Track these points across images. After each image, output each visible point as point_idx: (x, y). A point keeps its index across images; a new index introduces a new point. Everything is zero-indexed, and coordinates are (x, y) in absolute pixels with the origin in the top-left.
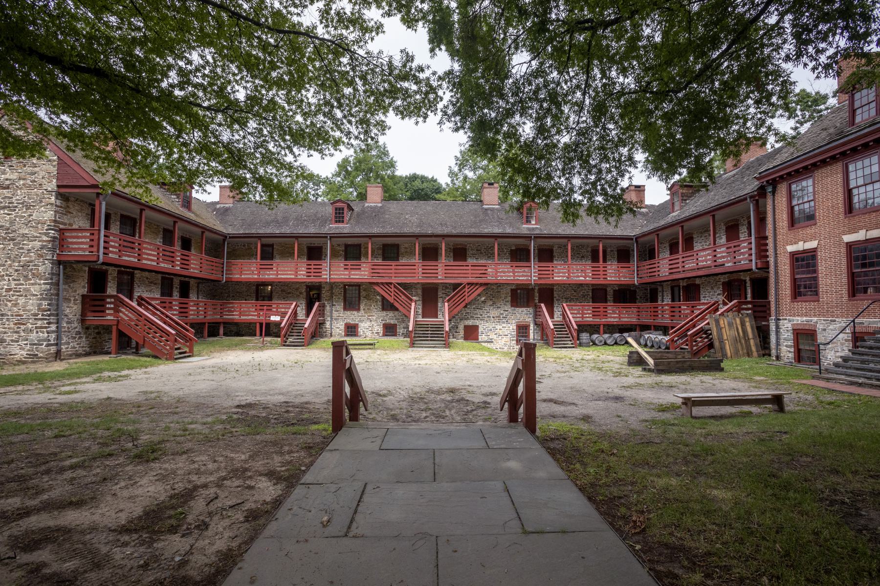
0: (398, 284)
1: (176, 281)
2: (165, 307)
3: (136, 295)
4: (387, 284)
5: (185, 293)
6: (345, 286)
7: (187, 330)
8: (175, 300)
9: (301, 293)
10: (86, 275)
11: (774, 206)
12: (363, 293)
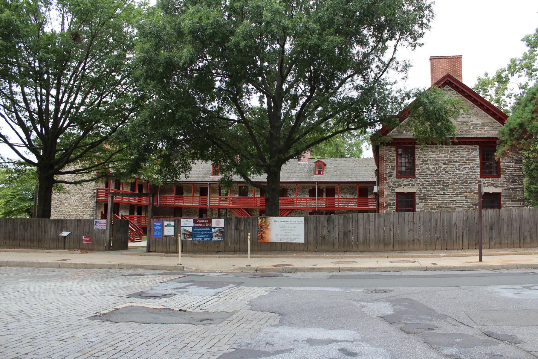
1: (136, 207)
3: (120, 214)
4: (238, 209)
5: (139, 213)
6: (219, 209)
7: (140, 230)
8: (135, 216)
9: (196, 213)
10: (104, 206)
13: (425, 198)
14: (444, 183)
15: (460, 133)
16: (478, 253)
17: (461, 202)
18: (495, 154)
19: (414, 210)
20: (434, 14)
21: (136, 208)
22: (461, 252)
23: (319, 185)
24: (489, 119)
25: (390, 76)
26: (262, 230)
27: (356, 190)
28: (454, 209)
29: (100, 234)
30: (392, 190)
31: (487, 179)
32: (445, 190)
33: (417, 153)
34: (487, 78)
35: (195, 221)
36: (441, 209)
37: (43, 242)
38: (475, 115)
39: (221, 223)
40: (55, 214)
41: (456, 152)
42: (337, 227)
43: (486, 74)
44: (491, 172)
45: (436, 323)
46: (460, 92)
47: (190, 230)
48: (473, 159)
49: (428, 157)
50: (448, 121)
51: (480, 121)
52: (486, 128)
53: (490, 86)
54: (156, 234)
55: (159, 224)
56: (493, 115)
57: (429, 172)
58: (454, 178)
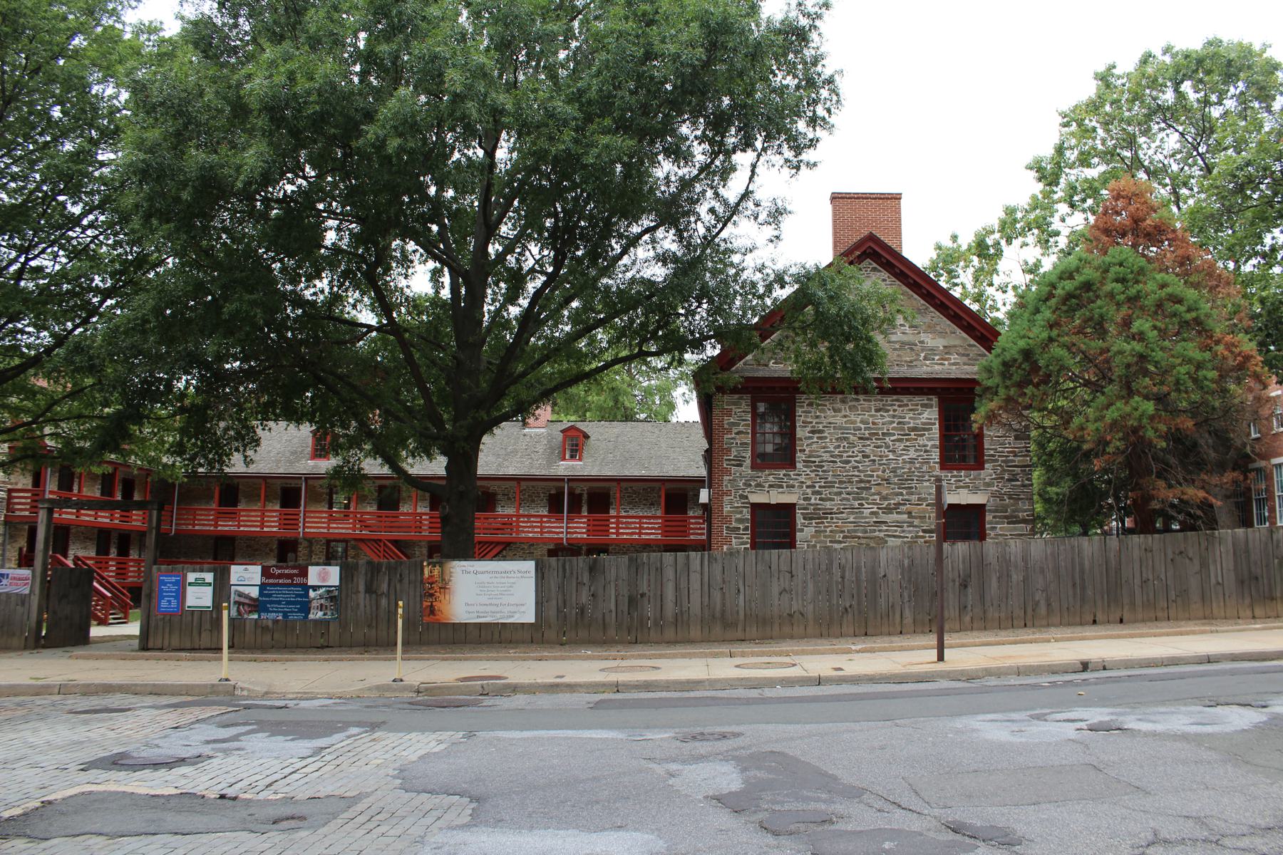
0: (389, 541)
2: (100, 568)
4: (375, 541)
5: (124, 551)
7: (124, 594)
8: (112, 559)
9: (271, 550)
11: (996, 721)
13: (816, 516)
14: (861, 481)
15: (896, 368)
17: (899, 524)
18: (973, 417)
19: (792, 544)
20: (841, 99)
22: (898, 641)
23: (571, 484)
24: (960, 338)
26: (432, 592)
27: (660, 497)
30: (742, 497)
31: (955, 473)
32: (863, 499)
33: (799, 411)
34: (955, 245)
36: (854, 542)
38: (931, 329)
39: (333, 575)
41: (888, 411)
47: (254, 592)
48: (925, 428)
49: (825, 421)
50: (869, 340)
51: (939, 343)
52: (954, 358)
53: (962, 264)
54: (164, 604)
55: (174, 579)
57: (826, 457)
58: (884, 471)
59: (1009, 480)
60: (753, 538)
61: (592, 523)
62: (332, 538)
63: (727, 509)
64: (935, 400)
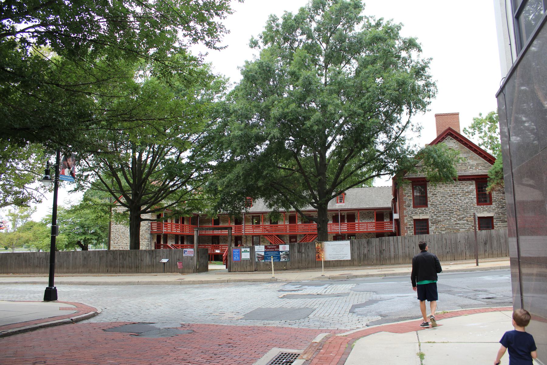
1: (180, 237)
4: (271, 235)
12: (261, 240)
13: (436, 222)
14: (450, 210)
15: (460, 172)
16: (476, 261)
17: (464, 224)
18: (486, 189)
19: (428, 233)
20: (438, 90)
21: (180, 238)
22: (464, 261)
23: (341, 212)
24: (482, 160)
25: (407, 134)
26: (318, 252)
27: (373, 215)
28: (458, 230)
29: (189, 260)
30: (410, 217)
31: (482, 206)
32: (451, 216)
33: (428, 188)
34: (481, 117)
35: (266, 247)
36: (449, 231)
37: (140, 268)
38: (471, 158)
39: (287, 248)
40: (113, 246)
41: (458, 186)
42: (374, 247)
43: (480, 114)
44: (486, 201)
45: (452, 289)
46: (458, 141)
47: (263, 254)
48: (472, 192)
49: (437, 191)
50: (451, 167)
51: (475, 163)
52: (480, 167)
53: (484, 124)
54: (235, 258)
55: (237, 251)
56: (485, 158)
57: (438, 203)
58: (458, 207)
59: (501, 208)
60: (415, 231)
61: (349, 226)
62: (254, 235)
63: (406, 221)
64: (474, 182)
